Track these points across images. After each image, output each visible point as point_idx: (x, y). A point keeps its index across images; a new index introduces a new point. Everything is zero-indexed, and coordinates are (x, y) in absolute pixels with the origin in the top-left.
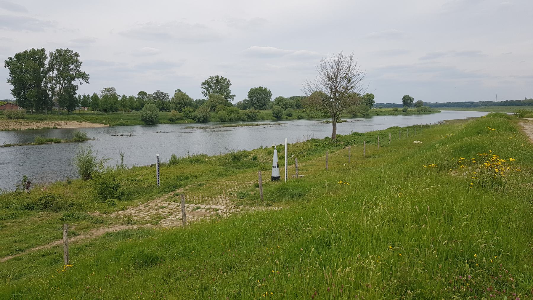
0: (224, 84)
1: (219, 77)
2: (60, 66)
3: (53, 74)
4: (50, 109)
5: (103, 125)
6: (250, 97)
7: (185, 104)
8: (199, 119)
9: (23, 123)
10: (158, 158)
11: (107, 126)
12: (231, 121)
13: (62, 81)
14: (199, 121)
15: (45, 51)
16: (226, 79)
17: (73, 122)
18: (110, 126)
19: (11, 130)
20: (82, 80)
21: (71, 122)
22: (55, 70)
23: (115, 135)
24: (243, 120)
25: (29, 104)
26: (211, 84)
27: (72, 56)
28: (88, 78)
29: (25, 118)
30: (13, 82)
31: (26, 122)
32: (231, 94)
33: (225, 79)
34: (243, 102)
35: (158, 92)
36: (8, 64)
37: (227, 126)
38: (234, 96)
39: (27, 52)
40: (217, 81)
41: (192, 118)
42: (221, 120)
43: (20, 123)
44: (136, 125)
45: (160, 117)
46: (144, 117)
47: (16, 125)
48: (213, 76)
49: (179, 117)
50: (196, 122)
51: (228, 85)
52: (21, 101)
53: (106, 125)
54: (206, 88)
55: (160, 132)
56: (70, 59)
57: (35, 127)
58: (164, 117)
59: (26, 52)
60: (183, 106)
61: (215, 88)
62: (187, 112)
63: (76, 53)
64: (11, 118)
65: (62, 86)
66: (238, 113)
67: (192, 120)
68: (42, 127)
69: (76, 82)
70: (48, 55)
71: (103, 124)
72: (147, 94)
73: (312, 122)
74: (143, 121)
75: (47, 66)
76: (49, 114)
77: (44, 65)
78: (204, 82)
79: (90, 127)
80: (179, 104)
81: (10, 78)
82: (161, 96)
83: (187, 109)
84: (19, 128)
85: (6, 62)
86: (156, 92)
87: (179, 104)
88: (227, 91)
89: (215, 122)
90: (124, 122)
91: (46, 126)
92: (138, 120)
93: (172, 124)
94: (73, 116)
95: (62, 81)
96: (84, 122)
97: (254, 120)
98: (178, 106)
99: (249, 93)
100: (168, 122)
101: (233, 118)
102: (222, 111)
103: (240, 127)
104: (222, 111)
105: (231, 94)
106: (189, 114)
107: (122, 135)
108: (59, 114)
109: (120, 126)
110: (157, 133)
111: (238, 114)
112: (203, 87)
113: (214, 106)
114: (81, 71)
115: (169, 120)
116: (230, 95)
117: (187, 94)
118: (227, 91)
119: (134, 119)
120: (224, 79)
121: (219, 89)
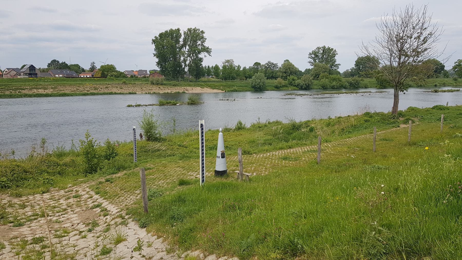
0: (330, 53)
1: (325, 47)
2: (190, 42)
3: (186, 49)
4: (183, 78)
5: (220, 91)
6: (356, 65)
7: (291, 73)
8: (302, 87)
9: (161, 88)
10: (135, 131)
11: (223, 91)
12: (333, 88)
13: (191, 55)
14: (302, 89)
15: (180, 31)
16: (332, 49)
17: (197, 88)
18: (225, 91)
19: (153, 93)
20: (206, 54)
21: (196, 88)
22: (187, 45)
23: (222, 100)
24: (345, 88)
25: (168, 73)
26: (318, 54)
27: (199, 34)
28: (210, 51)
29: (163, 84)
30: (157, 56)
31: (164, 88)
32: (336, 63)
33: (332, 48)
34: (350, 71)
35: (269, 62)
36: (154, 41)
37: (325, 94)
38: (340, 65)
39: (167, 31)
40: (323, 51)
41: (295, 86)
42: (323, 88)
43: (159, 88)
44: (246, 91)
45: (267, 85)
46: (253, 85)
47: (156, 89)
48: (320, 47)
49: (284, 84)
50: (299, 89)
51: (334, 55)
52: (163, 72)
53: (223, 91)
54: (313, 58)
55: (261, 98)
56: (197, 36)
57: (169, 91)
58: (271, 84)
59: (166, 32)
60: (289, 74)
61: (321, 58)
62: (291, 80)
63: (202, 31)
64: (154, 84)
65: (192, 59)
66: (340, 81)
67: (295, 87)
68: (174, 92)
69: (201, 55)
70: (182, 34)
71: (220, 90)
72: (261, 64)
73: (419, 90)
74: (252, 88)
75: (181, 43)
76: (182, 81)
77: (179, 41)
78: (311, 52)
79: (210, 92)
80: (285, 72)
81: (155, 52)
82: (272, 66)
83: (292, 77)
84: (158, 92)
85: (153, 40)
86: (267, 62)
87: (285, 72)
88: (333, 60)
89: (317, 89)
90: (237, 89)
91: (177, 91)
92: (249, 87)
93: (277, 90)
94: (198, 83)
95: (191, 55)
96: (206, 88)
97: (357, 87)
98: (285, 75)
99: (356, 61)
100: (274, 88)
101: (335, 86)
102: (325, 79)
103: (338, 94)
104: (325, 79)
105: (336, 63)
106: (293, 82)
107: (228, 100)
108: (189, 81)
109: (234, 92)
110: (261, 99)
111: (341, 82)
112: (310, 57)
113: (317, 75)
114: (206, 46)
115: (274, 87)
116: (335, 64)
117: (293, 64)
118: (333, 60)
119: (245, 86)
120: (330, 48)
121: (325, 58)
